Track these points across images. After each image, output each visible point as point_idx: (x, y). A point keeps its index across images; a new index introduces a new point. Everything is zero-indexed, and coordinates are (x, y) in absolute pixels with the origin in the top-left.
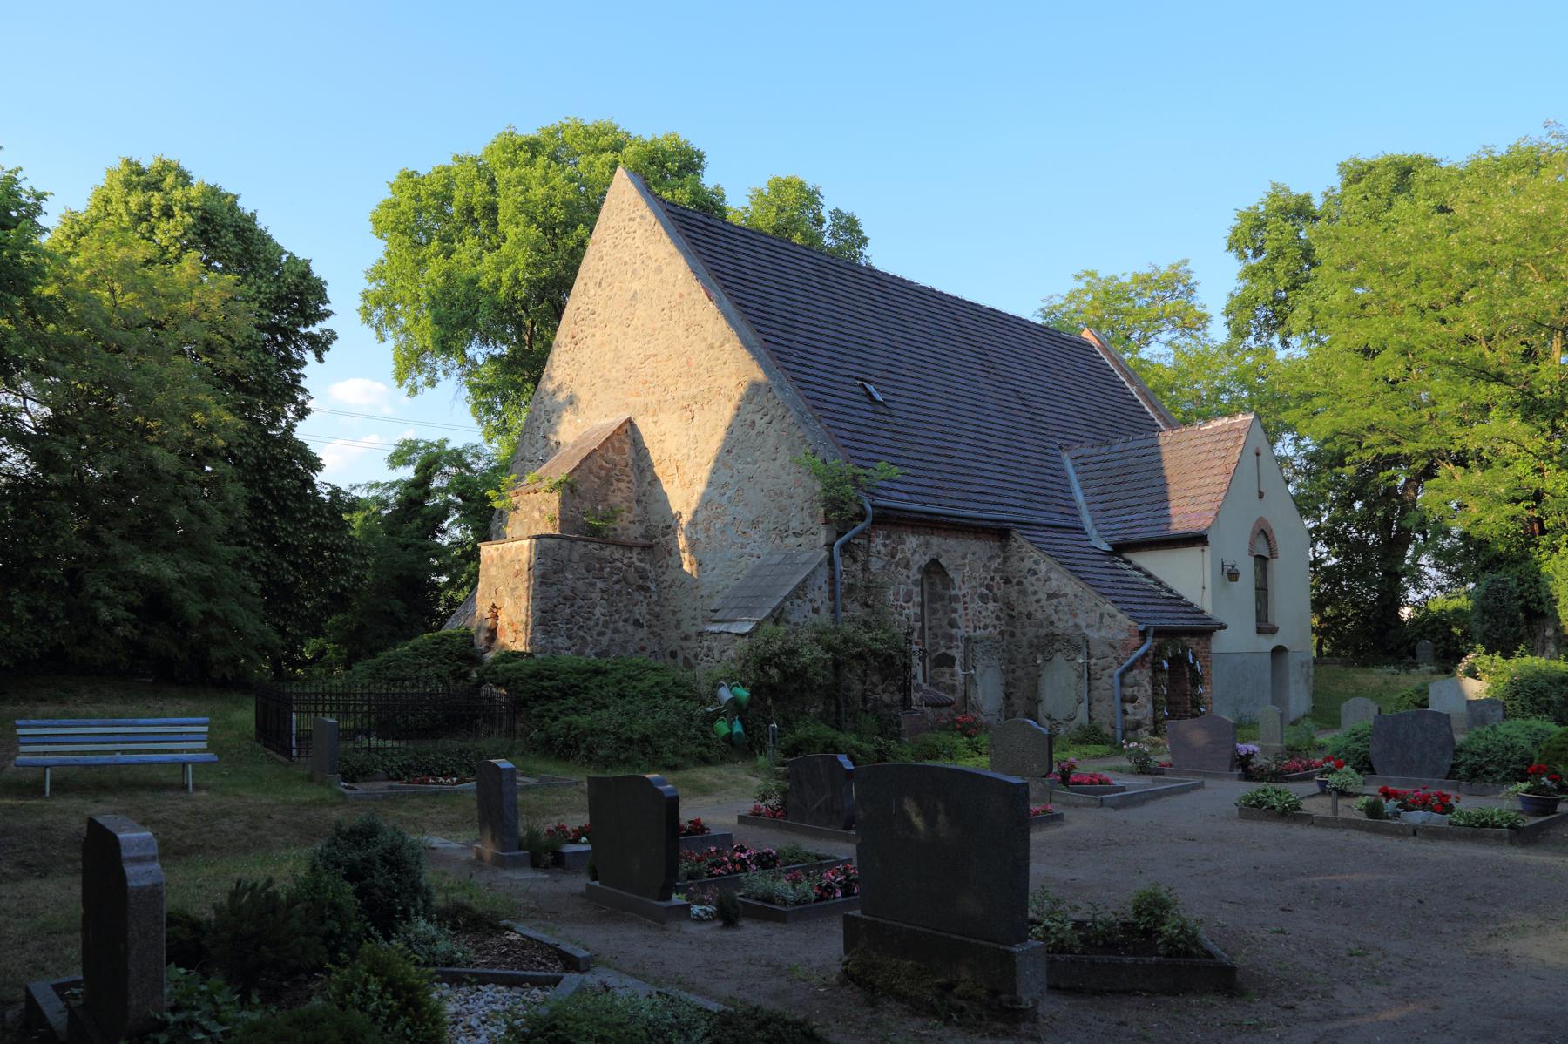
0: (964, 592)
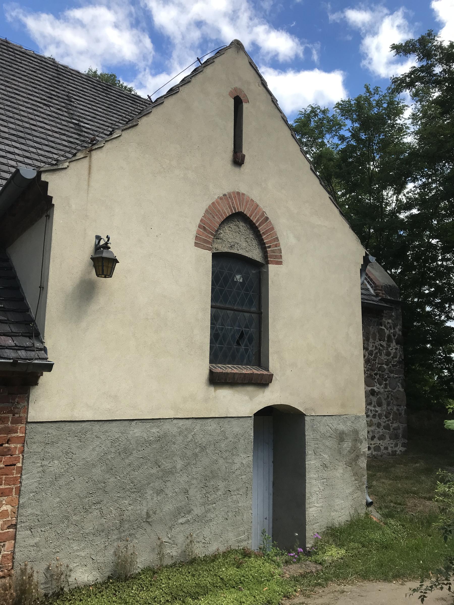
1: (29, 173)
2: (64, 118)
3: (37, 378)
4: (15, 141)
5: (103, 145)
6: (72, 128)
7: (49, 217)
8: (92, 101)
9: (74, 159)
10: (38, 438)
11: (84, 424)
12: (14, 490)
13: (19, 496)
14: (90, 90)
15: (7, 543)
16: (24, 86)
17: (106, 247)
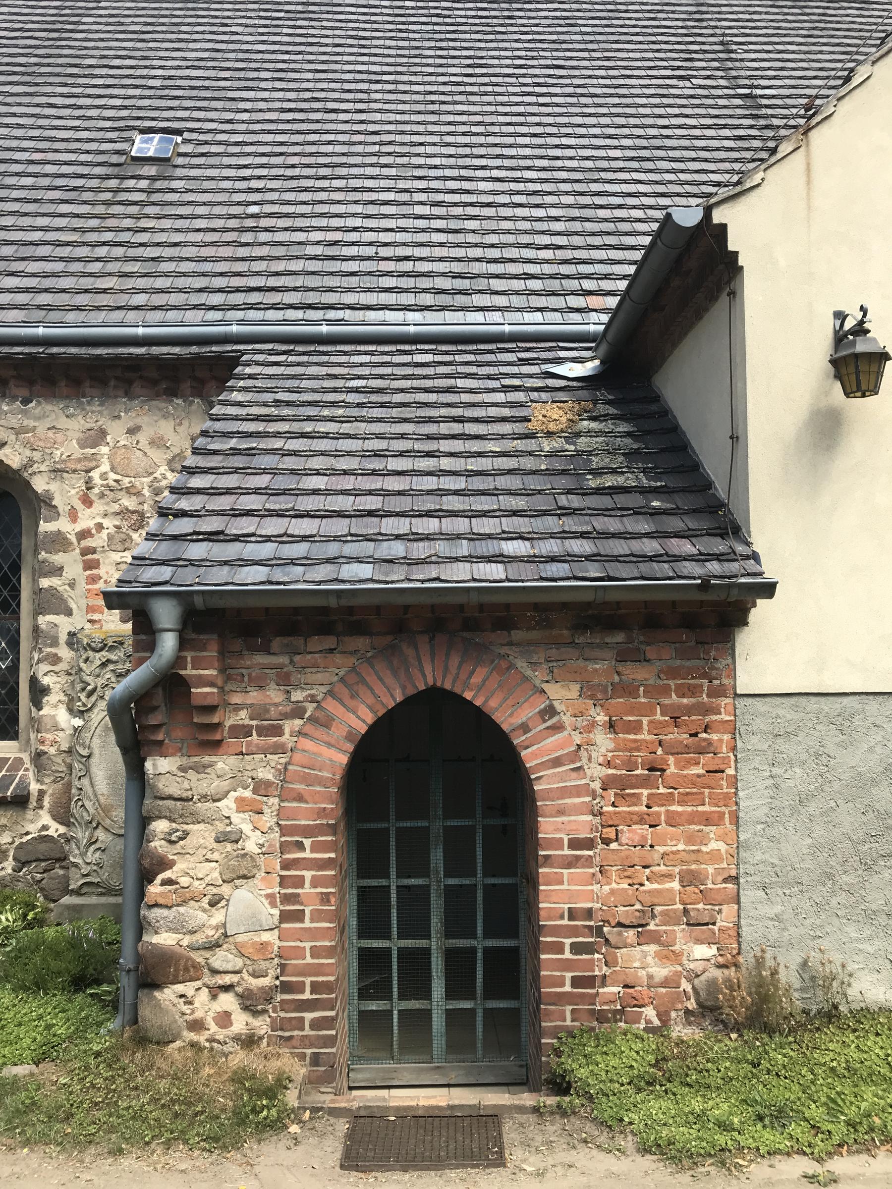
0: (86, 521)
1: (688, 216)
2: (719, 92)
3: (745, 612)
4: (636, 170)
5: (833, 109)
6: (738, 107)
7: (734, 294)
8: (773, 35)
9: (773, 160)
10: (758, 724)
11: (845, 700)
12: (727, 816)
13: (738, 828)
14: (766, 13)
15: (725, 908)
16: (638, 55)
17: (860, 330)
